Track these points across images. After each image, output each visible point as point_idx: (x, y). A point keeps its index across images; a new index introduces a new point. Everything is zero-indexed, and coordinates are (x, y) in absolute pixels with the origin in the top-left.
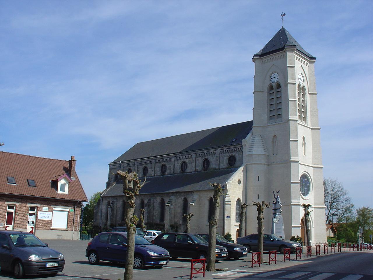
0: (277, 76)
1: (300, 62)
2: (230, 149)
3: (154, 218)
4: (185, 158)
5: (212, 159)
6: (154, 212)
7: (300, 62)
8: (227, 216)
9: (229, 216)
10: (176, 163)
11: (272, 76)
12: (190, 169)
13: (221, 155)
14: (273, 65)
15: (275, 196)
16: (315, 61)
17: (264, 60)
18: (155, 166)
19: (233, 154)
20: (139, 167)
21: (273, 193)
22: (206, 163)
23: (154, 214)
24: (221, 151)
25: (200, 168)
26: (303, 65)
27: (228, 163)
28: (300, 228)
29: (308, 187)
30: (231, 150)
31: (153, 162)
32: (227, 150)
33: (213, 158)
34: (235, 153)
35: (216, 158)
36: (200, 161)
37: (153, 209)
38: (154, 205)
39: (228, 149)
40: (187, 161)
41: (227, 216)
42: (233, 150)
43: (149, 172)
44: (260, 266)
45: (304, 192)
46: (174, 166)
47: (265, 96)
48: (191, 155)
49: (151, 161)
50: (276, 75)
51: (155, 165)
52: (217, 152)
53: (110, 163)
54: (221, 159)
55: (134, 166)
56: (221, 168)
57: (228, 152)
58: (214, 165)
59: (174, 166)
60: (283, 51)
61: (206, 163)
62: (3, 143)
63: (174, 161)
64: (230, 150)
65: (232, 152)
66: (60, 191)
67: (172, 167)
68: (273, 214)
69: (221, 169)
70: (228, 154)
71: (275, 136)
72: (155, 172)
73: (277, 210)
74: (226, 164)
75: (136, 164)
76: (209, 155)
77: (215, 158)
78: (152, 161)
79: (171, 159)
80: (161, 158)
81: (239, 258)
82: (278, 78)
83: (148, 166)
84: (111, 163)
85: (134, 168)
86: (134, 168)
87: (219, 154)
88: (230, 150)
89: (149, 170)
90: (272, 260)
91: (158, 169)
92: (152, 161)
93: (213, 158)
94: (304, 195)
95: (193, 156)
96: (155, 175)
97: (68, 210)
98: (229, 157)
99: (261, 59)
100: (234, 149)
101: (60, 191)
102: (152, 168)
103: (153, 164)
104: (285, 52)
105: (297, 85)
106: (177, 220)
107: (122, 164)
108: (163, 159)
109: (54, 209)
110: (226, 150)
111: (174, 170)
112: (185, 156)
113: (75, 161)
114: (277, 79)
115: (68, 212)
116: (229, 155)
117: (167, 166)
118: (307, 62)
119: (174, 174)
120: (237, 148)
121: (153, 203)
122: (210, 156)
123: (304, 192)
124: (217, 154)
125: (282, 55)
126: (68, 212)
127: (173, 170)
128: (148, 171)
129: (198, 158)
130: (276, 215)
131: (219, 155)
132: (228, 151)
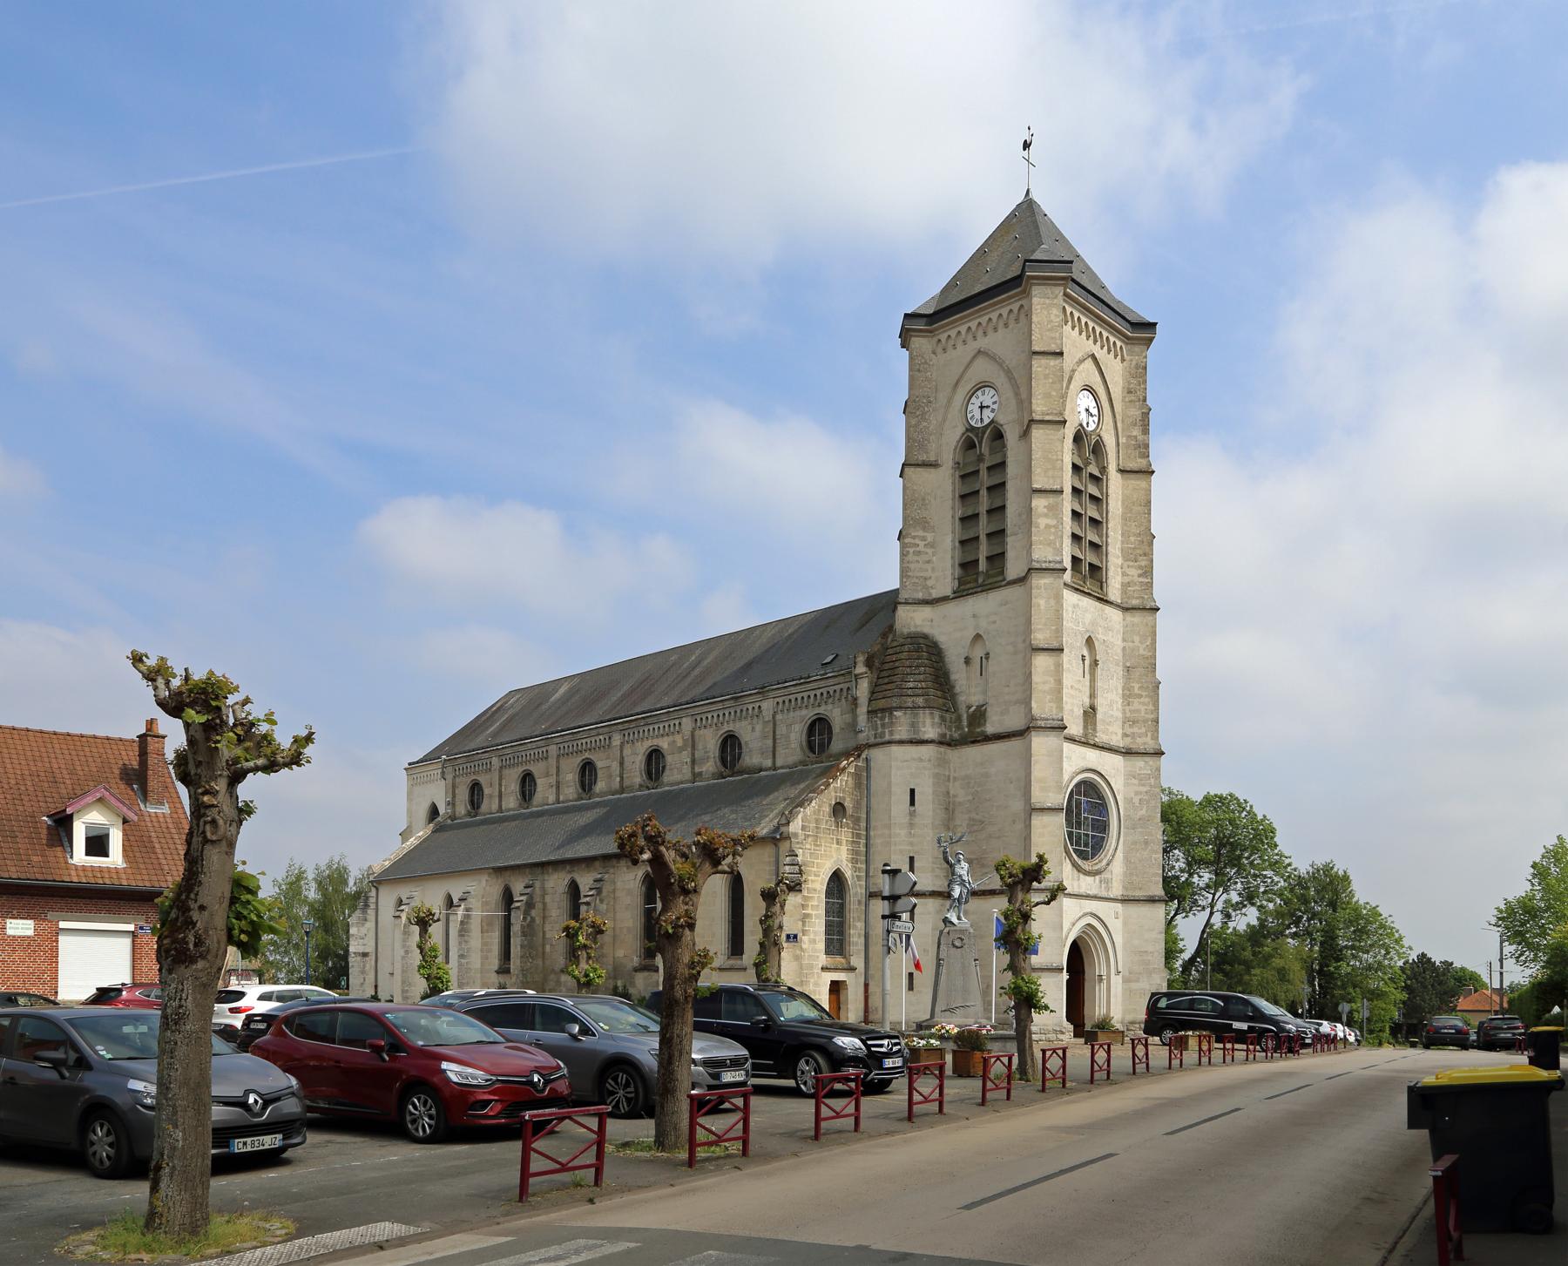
0: (994, 399)
1: (1073, 328)
2: (812, 694)
3: (548, 948)
4: (661, 731)
5: (752, 736)
6: (547, 927)
7: (1073, 328)
8: (788, 936)
9: (795, 936)
10: (627, 751)
11: (972, 401)
12: (677, 772)
13: (779, 717)
14: (979, 352)
15: (945, 853)
16: (1151, 340)
17: (943, 337)
18: (558, 768)
19: (821, 710)
20: (506, 772)
21: (1390, 916)
22: (730, 744)
23: (547, 936)
24: (780, 700)
25: (710, 766)
26: (1101, 354)
27: (804, 744)
28: (1065, 976)
29: (1102, 827)
30: (815, 695)
31: (550, 753)
32: (803, 698)
33: (753, 728)
34: (830, 707)
35: (763, 729)
36: (710, 742)
37: (544, 918)
38: (544, 904)
39: (805, 695)
40: (664, 744)
41: (788, 936)
42: (822, 694)
43: (539, 788)
44: (1012, 1098)
45: (1086, 845)
46: (622, 764)
47: (941, 484)
48: (677, 722)
49: (544, 749)
50: (987, 397)
51: (558, 761)
52: (767, 706)
53: (410, 764)
54: (782, 730)
55: (490, 770)
56: (779, 763)
57: (818, 701)
58: (753, 756)
59: (622, 764)
60: (1020, 289)
61: (730, 744)
62: (1006, 856)
63: (622, 744)
64: (799, 699)
65: (819, 706)
66: (88, 853)
67: (615, 766)
68: (884, 917)
69: (782, 767)
70: (804, 712)
71: (978, 637)
72: (558, 787)
73: (900, 902)
74: (798, 749)
75: (495, 761)
76: (740, 719)
77: (759, 728)
78: (547, 751)
79: (610, 738)
80: (579, 736)
81: (1424, 1078)
82: (995, 407)
83: (536, 769)
84: (414, 763)
85: (488, 776)
86: (491, 779)
87: (772, 712)
88: (812, 697)
89: (539, 781)
90: (1051, 1076)
91: (571, 777)
92: (547, 751)
93: (753, 728)
94: (1083, 856)
95: (683, 726)
96: (561, 798)
97: (131, 927)
98: (809, 722)
99: (931, 332)
100: (824, 691)
101: (88, 853)
102: (547, 775)
103: (552, 761)
104: (1027, 294)
105: (1069, 432)
106: (622, 955)
107: (448, 764)
108: (584, 741)
109: (62, 925)
110: (799, 696)
111: (622, 778)
112: (656, 727)
113: (164, 737)
114: (993, 411)
115: (134, 934)
116: (808, 714)
117: (599, 764)
118: (1119, 344)
119: (622, 790)
120: (836, 687)
121: (543, 896)
122: (744, 723)
123: (1086, 845)
124: (767, 715)
125: (1015, 307)
126: (134, 934)
127: (618, 779)
128: (535, 784)
129: (703, 732)
130: (897, 923)
131: (774, 717)
132: (805, 699)
